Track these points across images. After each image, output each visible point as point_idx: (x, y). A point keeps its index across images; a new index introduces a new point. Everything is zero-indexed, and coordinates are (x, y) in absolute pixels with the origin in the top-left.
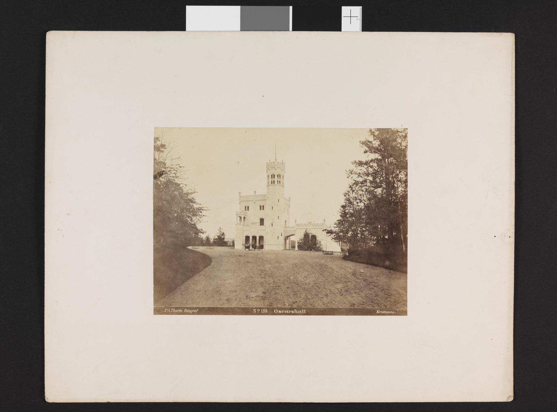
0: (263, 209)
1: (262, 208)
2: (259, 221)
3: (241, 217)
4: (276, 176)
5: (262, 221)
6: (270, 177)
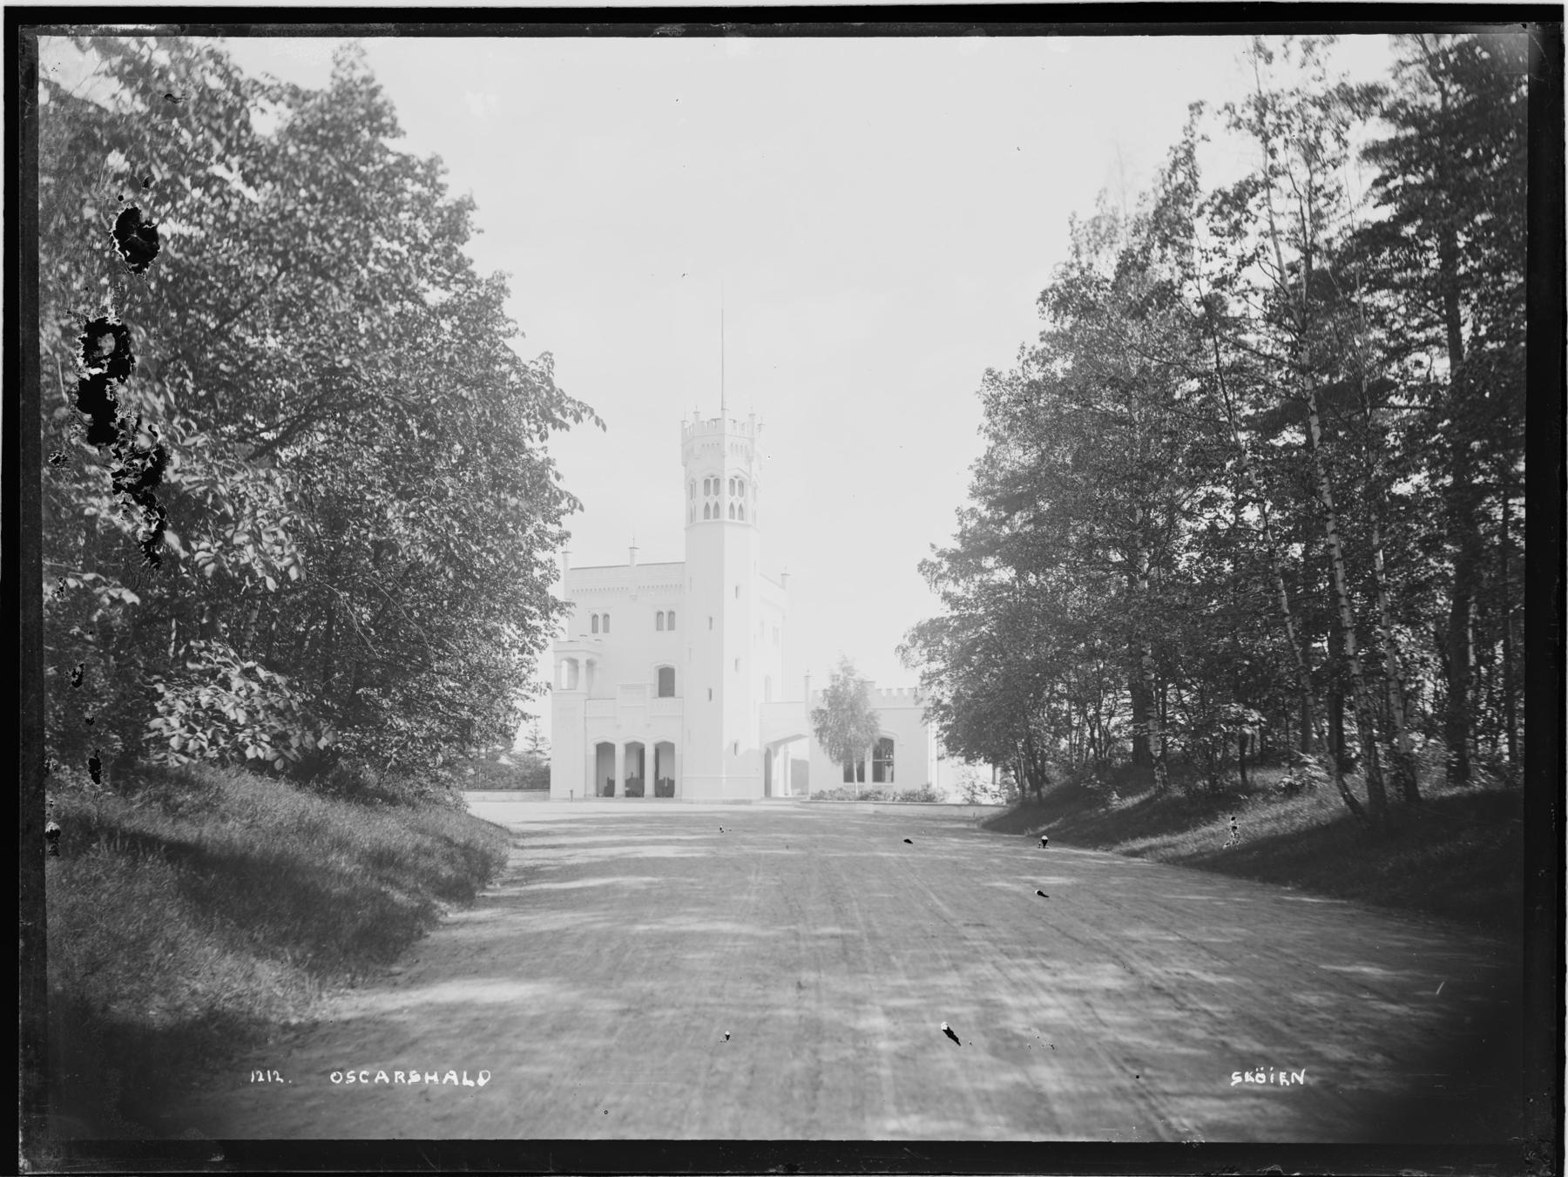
0: (671, 627)
1: (666, 620)
2: (652, 680)
3: (574, 663)
4: (725, 486)
5: (666, 682)
6: (700, 487)
